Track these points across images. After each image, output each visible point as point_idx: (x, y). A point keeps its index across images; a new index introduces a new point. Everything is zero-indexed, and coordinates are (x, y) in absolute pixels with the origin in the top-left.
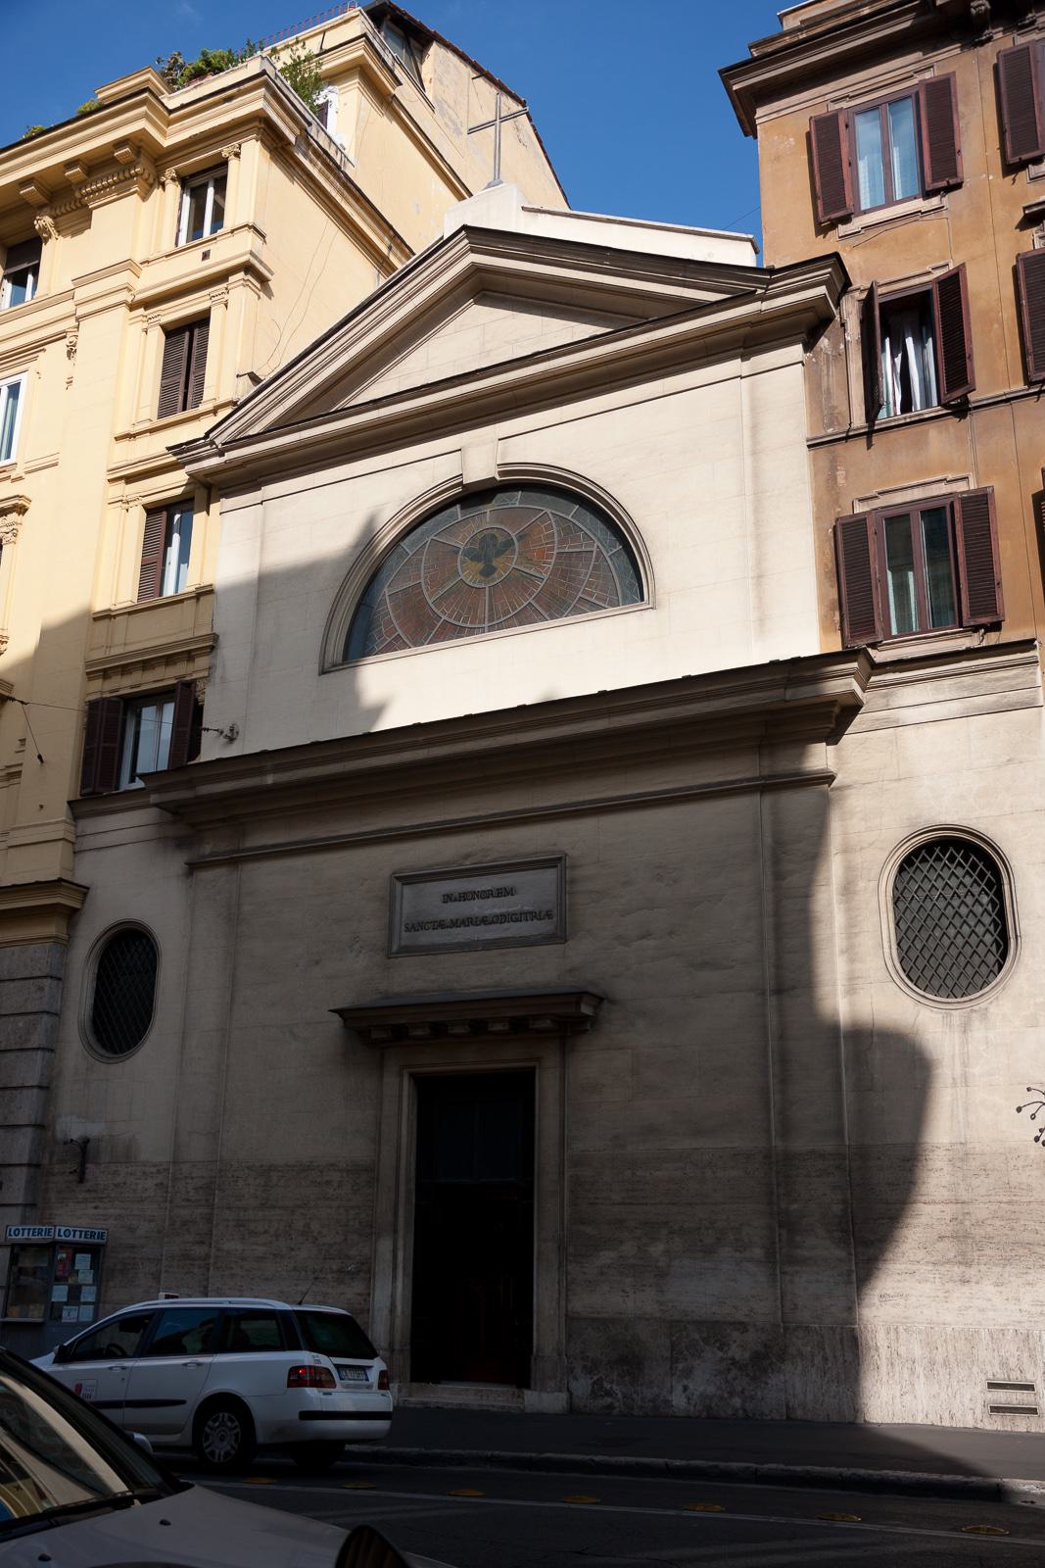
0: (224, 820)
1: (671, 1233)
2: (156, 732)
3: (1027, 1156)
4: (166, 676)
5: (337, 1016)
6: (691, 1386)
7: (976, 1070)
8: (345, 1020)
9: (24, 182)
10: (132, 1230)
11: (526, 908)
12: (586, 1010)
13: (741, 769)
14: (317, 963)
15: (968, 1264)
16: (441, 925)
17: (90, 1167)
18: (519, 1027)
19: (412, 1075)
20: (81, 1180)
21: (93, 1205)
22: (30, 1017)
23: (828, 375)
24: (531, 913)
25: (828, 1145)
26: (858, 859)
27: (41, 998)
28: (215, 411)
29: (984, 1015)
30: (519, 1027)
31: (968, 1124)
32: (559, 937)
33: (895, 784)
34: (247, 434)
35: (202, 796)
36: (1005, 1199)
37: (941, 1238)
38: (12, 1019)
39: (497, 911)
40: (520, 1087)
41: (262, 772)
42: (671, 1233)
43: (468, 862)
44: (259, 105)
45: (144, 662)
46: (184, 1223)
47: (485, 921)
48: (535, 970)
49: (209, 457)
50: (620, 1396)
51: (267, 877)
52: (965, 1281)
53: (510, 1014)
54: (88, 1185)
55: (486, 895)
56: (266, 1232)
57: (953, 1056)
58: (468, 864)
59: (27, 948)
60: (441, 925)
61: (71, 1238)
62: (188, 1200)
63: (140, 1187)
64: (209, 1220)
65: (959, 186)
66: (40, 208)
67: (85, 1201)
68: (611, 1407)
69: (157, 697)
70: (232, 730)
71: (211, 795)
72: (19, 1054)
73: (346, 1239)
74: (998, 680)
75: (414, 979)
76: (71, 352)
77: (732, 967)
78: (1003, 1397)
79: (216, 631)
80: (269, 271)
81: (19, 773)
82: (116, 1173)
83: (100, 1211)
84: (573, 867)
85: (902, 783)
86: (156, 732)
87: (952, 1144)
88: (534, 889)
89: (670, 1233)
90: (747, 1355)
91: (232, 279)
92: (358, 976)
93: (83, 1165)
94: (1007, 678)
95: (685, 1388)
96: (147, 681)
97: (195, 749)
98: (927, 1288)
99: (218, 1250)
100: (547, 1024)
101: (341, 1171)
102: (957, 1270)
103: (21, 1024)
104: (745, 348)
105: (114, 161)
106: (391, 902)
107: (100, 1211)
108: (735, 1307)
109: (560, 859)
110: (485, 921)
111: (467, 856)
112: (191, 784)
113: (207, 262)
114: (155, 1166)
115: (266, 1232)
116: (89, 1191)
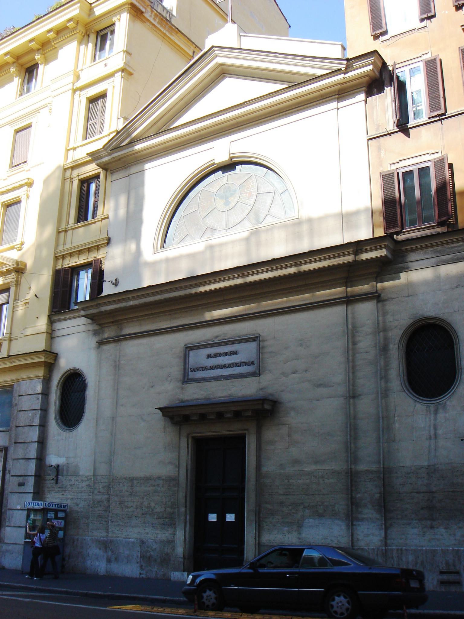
0: (113, 322)
1: (305, 507)
2: (85, 281)
3: (461, 471)
4: (91, 257)
5: (159, 410)
7: (440, 432)
8: (163, 413)
9: (31, 41)
10: (77, 504)
11: (243, 360)
12: (267, 407)
13: (337, 291)
14: (152, 387)
15: (433, 520)
16: (205, 369)
17: (60, 477)
18: (237, 415)
19: (193, 437)
20: (57, 483)
21: (61, 493)
22: (34, 411)
23: (376, 106)
24: (245, 362)
25: (374, 467)
26: (390, 334)
28: (109, 135)
29: (444, 407)
30: (237, 415)
31: (436, 456)
32: (257, 374)
33: (406, 299)
35: (102, 312)
36: (451, 490)
37: (422, 508)
38: (26, 412)
39: (230, 362)
40: (239, 441)
41: (127, 300)
42: (305, 507)
43: (217, 340)
45: (79, 251)
46: (99, 502)
47: (224, 366)
48: (246, 389)
49: (105, 156)
51: (132, 348)
52: (432, 527)
53: (234, 409)
54: (59, 485)
55: (226, 354)
56: (132, 506)
57: (430, 425)
58: (217, 340)
60: (205, 369)
61: (51, 507)
62: (100, 492)
63: (80, 486)
64: (108, 500)
65: (434, 16)
67: (59, 492)
69: (85, 266)
70: (116, 280)
71: (106, 311)
73: (165, 510)
74: (453, 248)
75: (194, 393)
76: (50, 112)
77: (333, 386)
78: (445, 577)
79: (109, 236)
80: (133, 70)
82: (70, 480)
83: (65, 496)
84: (264, 341)
85: (410, 298)
86: (85, 281)
87: (429, 466)
88: (247, 351)
89: (304, 508)
91: (116, 75)
92: (169, 392)
93: (57, 476)
94: (456, 247)
96: (82, 260)
97: (100, 290)
98: (415, 531)
99: (113, 514)
100: (249, 413)
101: (163, 480)
102: (429, 523)
103: (30, 414)
104: (339, 95)
105: (67, 28)
106: (186, 359)
107: (65, 496)
108: (332, 540)
109: (257, 337)
110: (224, 366)
111: (217, 337)
112: (97, 306)
114: (86, 477)
115: (132, 506)
116: (59, 487)
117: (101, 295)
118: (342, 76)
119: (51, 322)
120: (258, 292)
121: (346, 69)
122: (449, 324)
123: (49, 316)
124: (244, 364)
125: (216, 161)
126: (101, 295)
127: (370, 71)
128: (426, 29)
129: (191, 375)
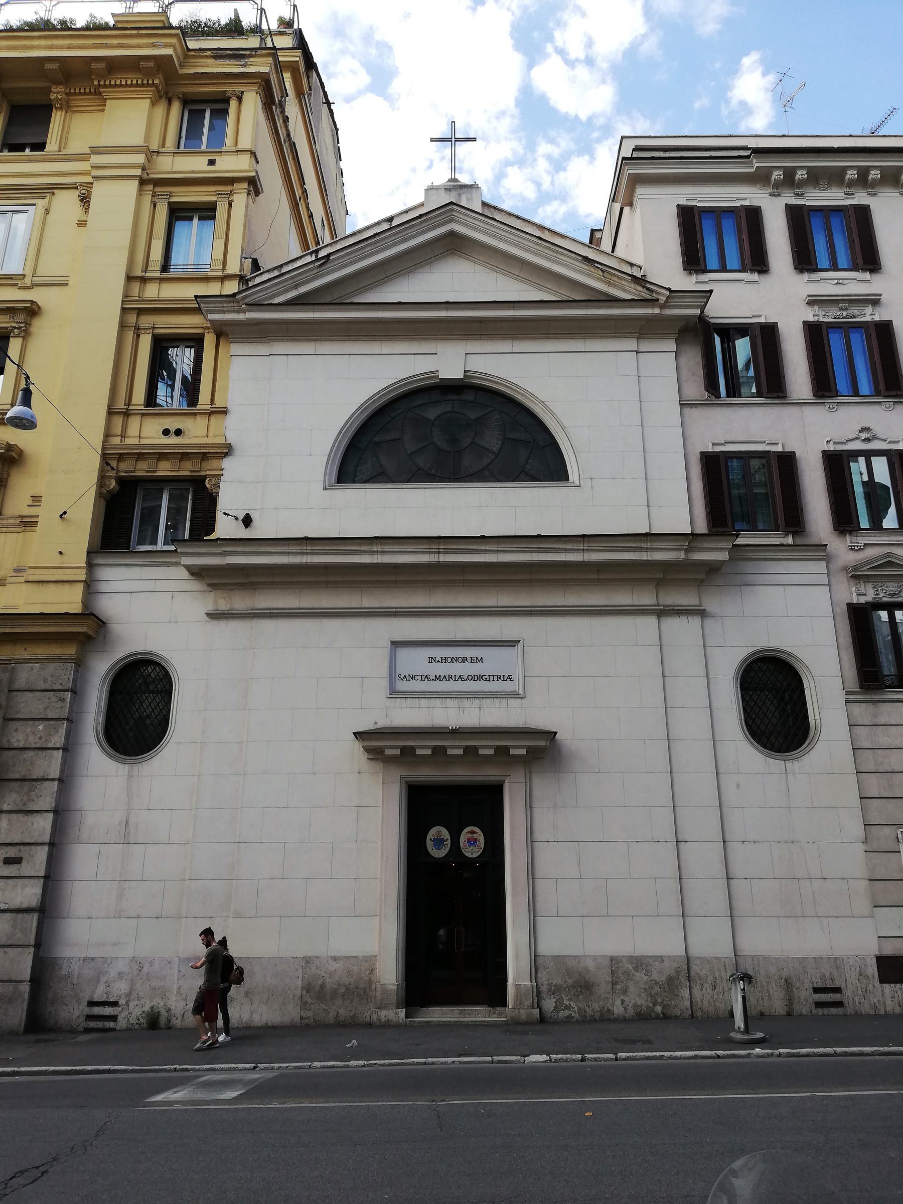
6: (627, 999)
13: (646, 598)
27: (62, 707)
34: (269, 302)
44: (266, 69)
50: (576, 1009)
59: (37, 669)
66: (57, 83)
68: (570, 1017)
72: (40, 752)
81: (35, 524)
90: (664, 978)
91: (237, 186)
95: (623, 1002)
113: (212, 168)
117: (212, 537)
118: (657, 311)
119: (91, 566)
120: (523, 577)
121: (666, 302)
122: (745, 660)
123: (88, 553)
124: (496, 678)
125: (442, 375)
126: (212, 537)
127: (693, 316)
128: (755, 285)
129: (402, 686)
